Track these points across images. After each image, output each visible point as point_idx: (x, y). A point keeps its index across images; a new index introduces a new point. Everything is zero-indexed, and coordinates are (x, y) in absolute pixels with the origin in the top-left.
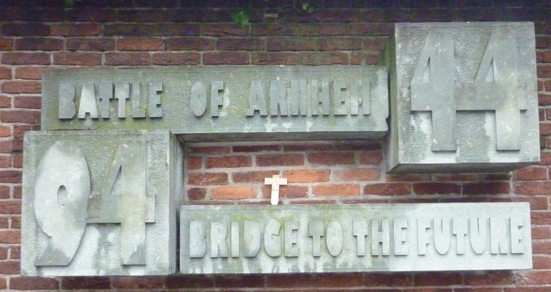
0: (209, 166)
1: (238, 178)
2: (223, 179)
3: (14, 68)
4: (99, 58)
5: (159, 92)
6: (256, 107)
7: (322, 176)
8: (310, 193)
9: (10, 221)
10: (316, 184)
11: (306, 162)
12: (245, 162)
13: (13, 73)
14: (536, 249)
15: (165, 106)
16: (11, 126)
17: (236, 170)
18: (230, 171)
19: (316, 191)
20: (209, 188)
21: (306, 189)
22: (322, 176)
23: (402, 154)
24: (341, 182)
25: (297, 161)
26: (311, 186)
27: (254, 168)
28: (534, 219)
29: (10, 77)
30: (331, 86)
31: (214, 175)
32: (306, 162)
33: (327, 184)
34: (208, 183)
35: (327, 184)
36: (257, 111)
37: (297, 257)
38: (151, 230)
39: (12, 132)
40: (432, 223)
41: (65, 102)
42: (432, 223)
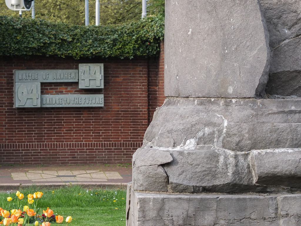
0: (45, 87)
1: (50, 89)
2: (47, 89)
3: (6, 67)
4: (22, 65)
5: (37, 75)
6: (54, 77)
7: (66, 89)
8: (64, 92)
9: (6, 97)
10: (65, 90)
11: (63, 86)
12: (52, 86)
13: (6, 68)
14: (105, 103)
15: (38, 77)
16: (6, 79)
17: (50, 87)
18: (48, 88)
19: (65, 91)
20: (45, 91)
21: (63, 91)
22: (66, 89)
23: (81, 86)
24: (70, 90)
25: (62, 86)
26: (64, 90)
27: (53, 87)
28: (104, 97)
29: (5, 69)
30: (68, 73)
31: (45, 88)
32: (63, 86)
33: (67, 90)
34: (44, 90)
35: (67, 90)
36: (55, 78)
37: (95, 80)
38: (38, 99)
39: (6, 80)
40: (86, 98)
41: (20, 76)
42: (86, 98)
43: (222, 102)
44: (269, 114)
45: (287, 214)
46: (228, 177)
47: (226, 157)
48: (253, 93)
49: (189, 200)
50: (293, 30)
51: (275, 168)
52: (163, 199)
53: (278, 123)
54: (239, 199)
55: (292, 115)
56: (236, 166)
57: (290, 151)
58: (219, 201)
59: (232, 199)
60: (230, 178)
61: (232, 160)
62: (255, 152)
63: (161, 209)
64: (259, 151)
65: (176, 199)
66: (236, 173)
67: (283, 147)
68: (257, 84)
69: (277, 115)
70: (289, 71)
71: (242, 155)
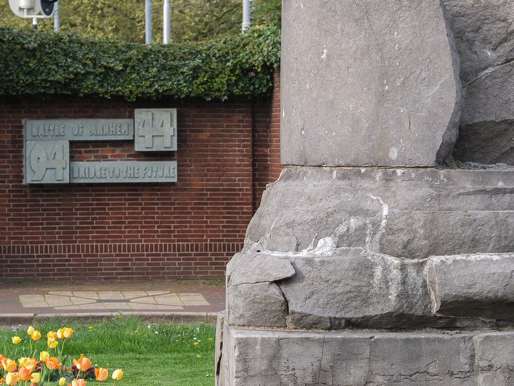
0: (76, 148)
1: (86, 152)
2: (80, 152)
3: (10, 115)
4: (38, 111)
5: (63, 128)
6: (93, 132)
7: (113, 151)
8: (109, 156)
9: (11, 166)
10: (111, 154)
11: (108, 147)
12: (88, 147)
13: (10, 117)
14: (178, 175)
15: (65, 132)
16: (10, 135)
17: (85, 149)
18: (83, 150)
19: (112, 156)
20: (76, 155)
21: (108, 156)
22: (113, 151)
23: (138, 147)
24: (120, 153)
25: (105, 147)
26: (109, 155)
27: (91, 149)
28: (178, 166)
29: (9, 118)
30: (116, 125)
31: (77, 151)
32: (108, 147)
33: (114, 154)
34: (75, 154)
35: (114, 154)
36: (93, 134)
37: (163, 136)
38: (64, 170)
39: (10, 136)
40: (146, 168)
41: (34, 130)
42: (146, 168)
43: (379, 174)
44: (460, 194)
45: (491, 366)
46: (390, 303)
47: (386, 269)
48: (431, 159)
49: (323, 342)
50: (501, 51)
51: (470, 287)
52: (279, 340)
53: (475, 210)
54: (408, 341)
55: (499, 197)
56: (404, 283)
57: (496, 257)
58: (374, 343)
59: (395, 340)
60: (393, 303)
61: (396, 274)
62: (435, 260)
63: (275, 357)
64: (443, 258)
65: (301, 339)
66: (403, 295)
67: (484, 251)
68: (439, 143)
69: (472, 197)
70: (493, 122)
71: (414, 264)
